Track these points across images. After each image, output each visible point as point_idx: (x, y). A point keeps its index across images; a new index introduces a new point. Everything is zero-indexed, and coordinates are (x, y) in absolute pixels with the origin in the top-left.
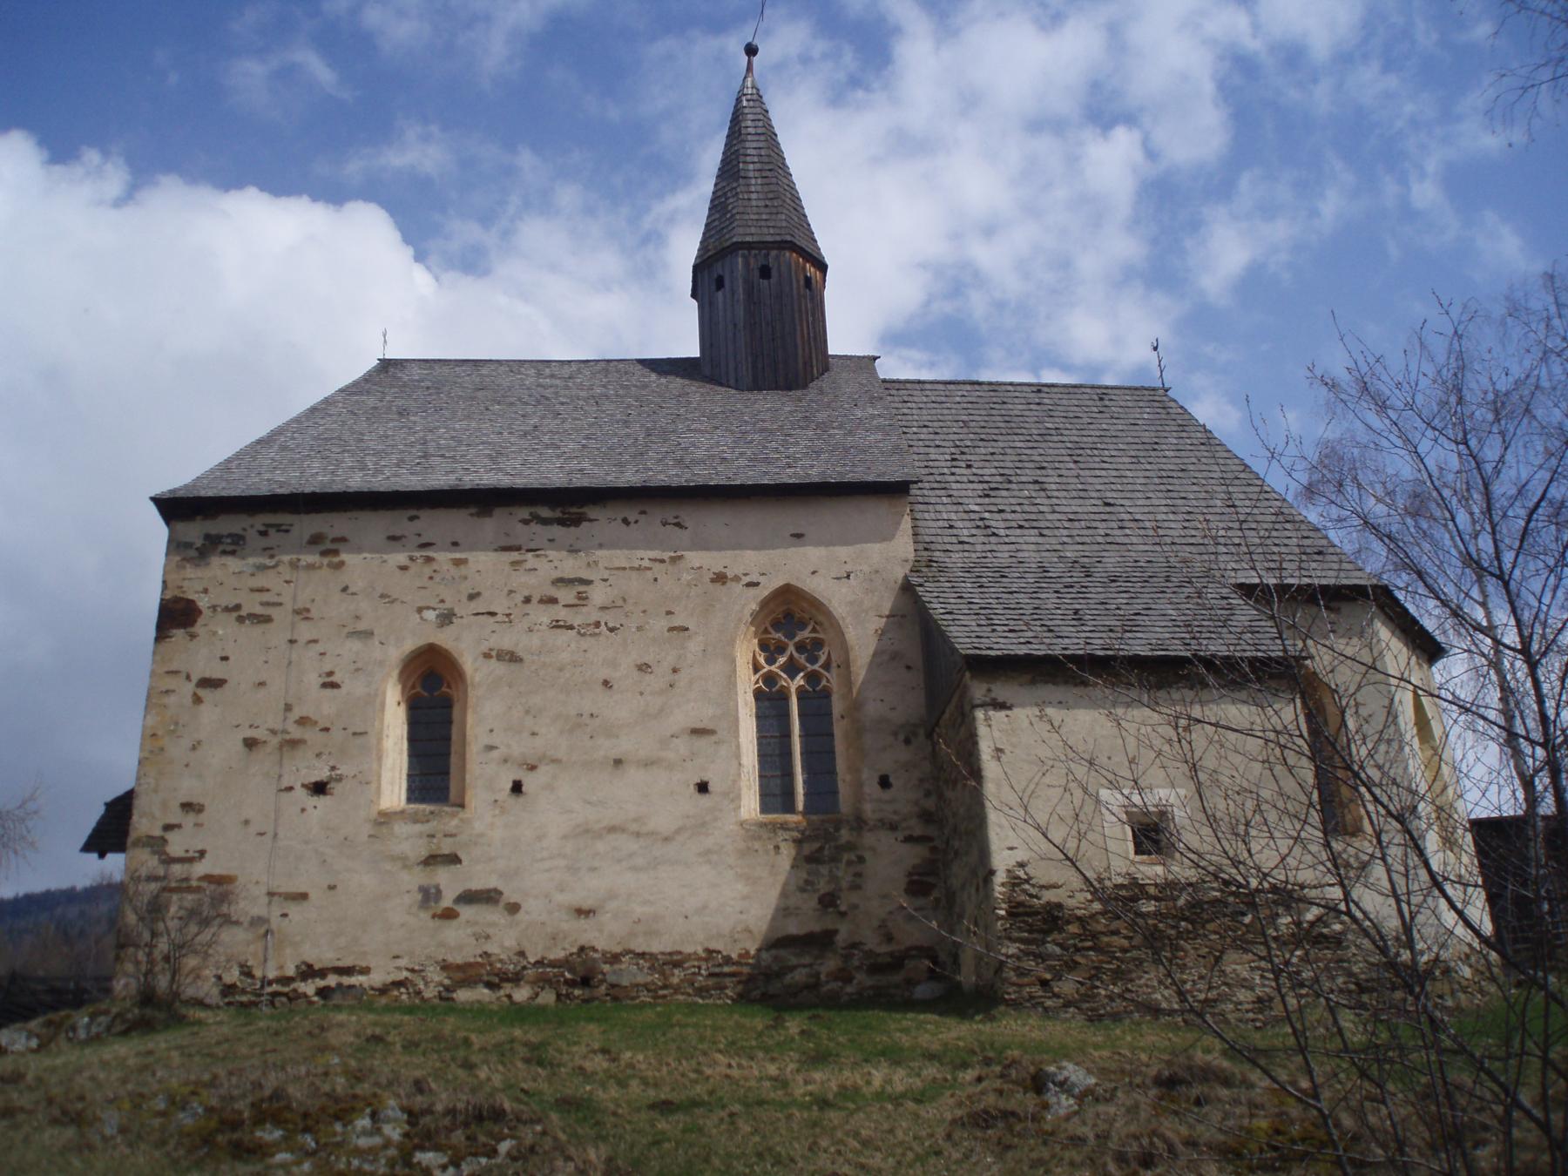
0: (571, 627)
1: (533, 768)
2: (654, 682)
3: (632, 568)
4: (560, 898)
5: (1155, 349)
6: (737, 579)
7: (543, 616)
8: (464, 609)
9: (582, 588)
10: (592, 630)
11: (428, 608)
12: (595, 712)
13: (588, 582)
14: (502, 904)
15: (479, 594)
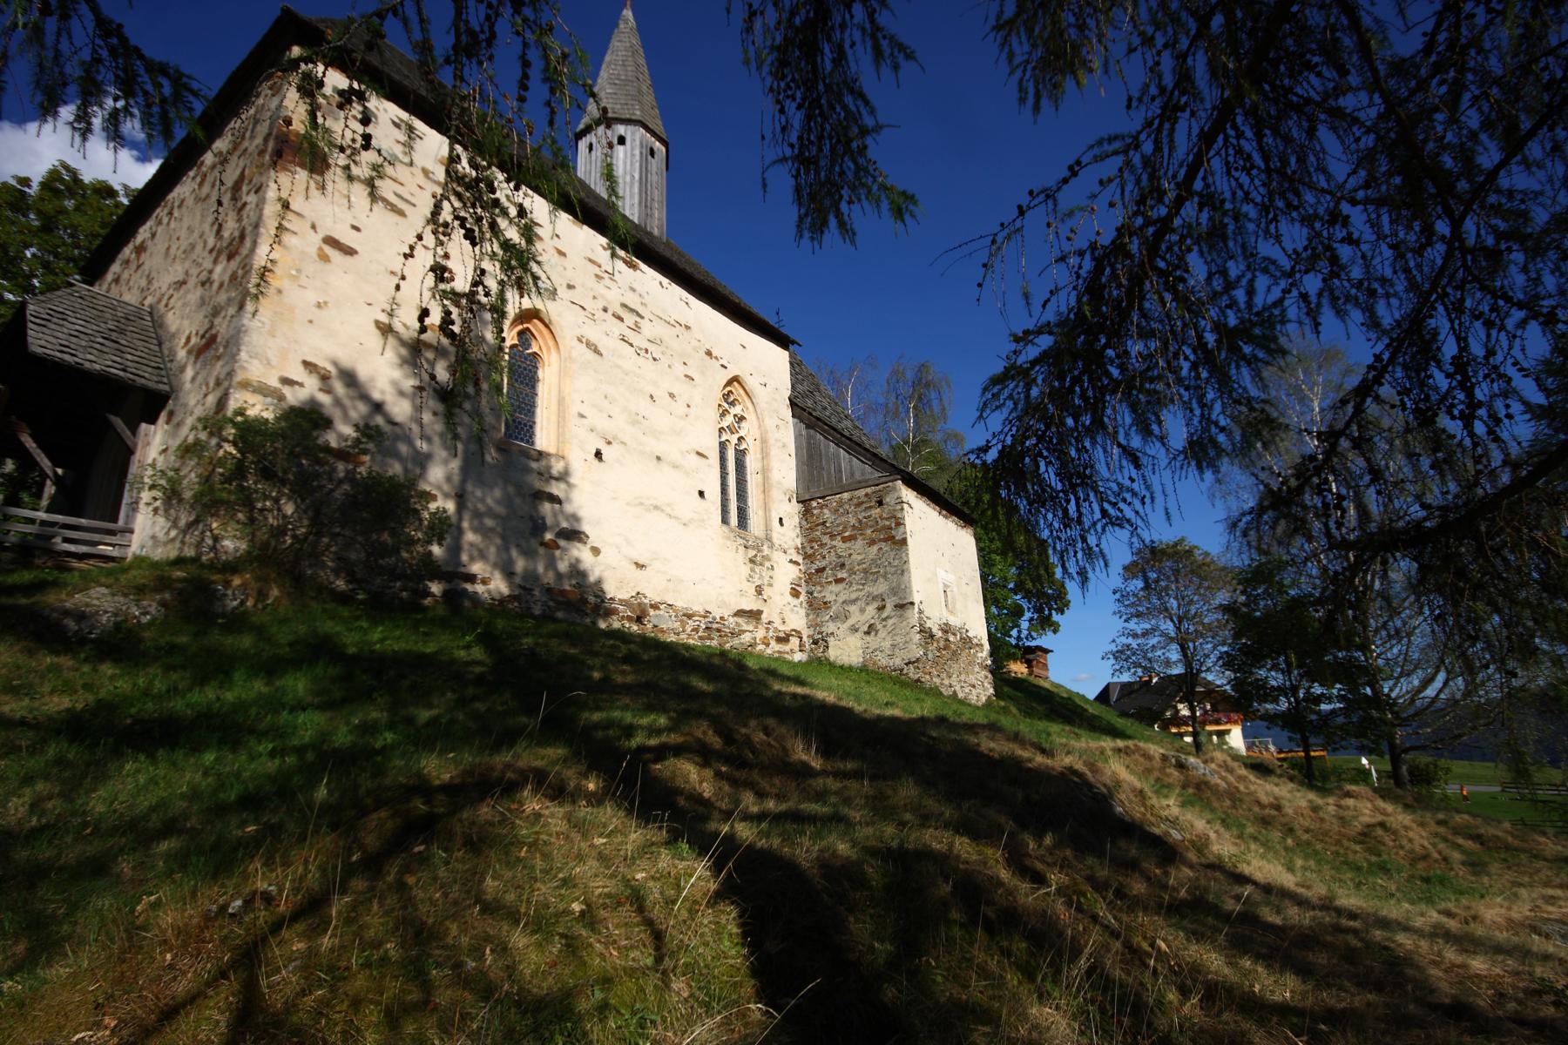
2: (679, 408)
7: (617, 328)
10: (642, 353)
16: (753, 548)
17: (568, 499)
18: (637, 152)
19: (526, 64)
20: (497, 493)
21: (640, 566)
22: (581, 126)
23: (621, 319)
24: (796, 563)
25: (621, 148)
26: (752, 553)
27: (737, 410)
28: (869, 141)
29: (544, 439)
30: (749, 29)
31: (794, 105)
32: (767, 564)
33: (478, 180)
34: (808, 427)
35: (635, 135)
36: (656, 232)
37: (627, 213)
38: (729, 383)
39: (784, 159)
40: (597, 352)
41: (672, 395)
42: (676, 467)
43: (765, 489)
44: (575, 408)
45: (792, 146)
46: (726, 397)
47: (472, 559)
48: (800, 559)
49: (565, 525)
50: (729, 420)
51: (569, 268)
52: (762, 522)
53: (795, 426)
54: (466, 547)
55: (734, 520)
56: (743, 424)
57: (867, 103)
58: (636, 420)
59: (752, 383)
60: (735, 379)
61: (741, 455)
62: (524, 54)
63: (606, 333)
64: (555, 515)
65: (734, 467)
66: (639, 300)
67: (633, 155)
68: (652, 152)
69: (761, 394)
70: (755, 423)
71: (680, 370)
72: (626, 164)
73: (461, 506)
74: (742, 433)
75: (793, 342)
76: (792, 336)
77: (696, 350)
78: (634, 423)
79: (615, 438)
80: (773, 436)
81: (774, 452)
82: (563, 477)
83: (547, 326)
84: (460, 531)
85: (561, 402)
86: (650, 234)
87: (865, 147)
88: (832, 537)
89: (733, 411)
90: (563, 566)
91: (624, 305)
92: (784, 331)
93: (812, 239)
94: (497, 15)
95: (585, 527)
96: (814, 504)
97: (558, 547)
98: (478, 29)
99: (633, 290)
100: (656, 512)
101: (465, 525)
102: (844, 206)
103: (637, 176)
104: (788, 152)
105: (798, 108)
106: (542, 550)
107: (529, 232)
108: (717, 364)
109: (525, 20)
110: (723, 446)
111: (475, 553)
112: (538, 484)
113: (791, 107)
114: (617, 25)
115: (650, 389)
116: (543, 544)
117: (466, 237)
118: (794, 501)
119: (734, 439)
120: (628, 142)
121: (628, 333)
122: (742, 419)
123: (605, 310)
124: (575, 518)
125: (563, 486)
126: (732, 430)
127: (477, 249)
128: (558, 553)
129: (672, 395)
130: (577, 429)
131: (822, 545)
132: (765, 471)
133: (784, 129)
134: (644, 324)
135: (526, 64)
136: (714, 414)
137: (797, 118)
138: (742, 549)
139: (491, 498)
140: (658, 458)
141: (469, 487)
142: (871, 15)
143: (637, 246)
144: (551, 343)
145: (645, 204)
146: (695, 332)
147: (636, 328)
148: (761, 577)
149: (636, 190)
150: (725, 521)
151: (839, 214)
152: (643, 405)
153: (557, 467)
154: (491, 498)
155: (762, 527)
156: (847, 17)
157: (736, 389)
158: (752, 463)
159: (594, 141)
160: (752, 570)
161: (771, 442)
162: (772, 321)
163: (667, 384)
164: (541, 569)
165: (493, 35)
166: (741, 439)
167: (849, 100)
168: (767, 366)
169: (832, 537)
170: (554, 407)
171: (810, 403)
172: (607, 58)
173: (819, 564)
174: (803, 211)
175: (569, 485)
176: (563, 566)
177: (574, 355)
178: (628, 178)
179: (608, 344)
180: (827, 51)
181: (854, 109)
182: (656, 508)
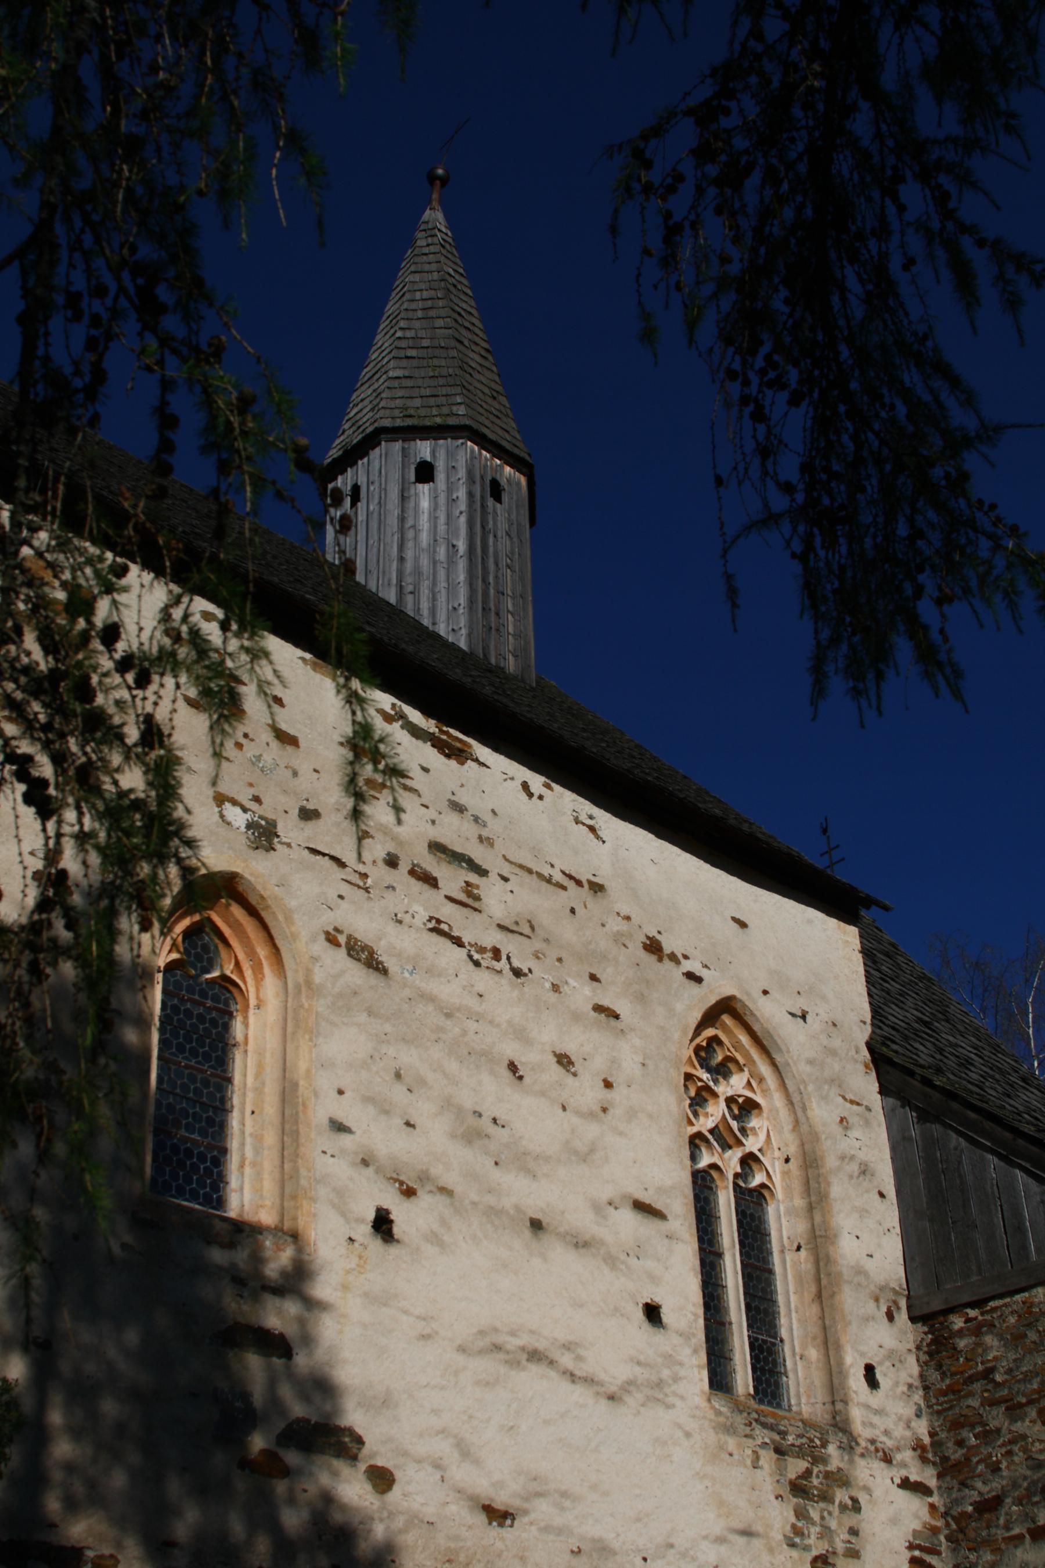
0: (458, 942)
1: (409, 1193)
2: (585, 1091)
3: (540, 875)
4: (462, 1474)
5: (825, 831)
6: (673, 957)
7: (422, 904)
8: (289, 829)
9: (473, 878)
10: (486, 960)
11: (234, 802)
12: (502, 1117)
13: (483, 873)
14: (362, 1467)
15: (870, 1110)
16: (800, 1452)
17: (308, 1340)
18: (461, 493)
19: (167, 421)
20: (132, 1337)
21: (498, 1515)
22: (334, 453)
23: (430, 881)
24: (918, 1488)
25: (424, 489)
26: (796, 1466)
27: (736, 1084)
28: (971, 461)
29: (249, 1191)
30: (669, 261)
31: (783, 396)
32: (841, 1496)
33: (55, 676)
34: (924, 1116)
35: (456, 459)
36: (511, 665)
37: (442, 630)
38: (710, 1017)
39: (770, 519)
40: (374, 964)
41: (564, 1061)
42: (581, 1244)
43: (824, 1285)
44: (323, 1108)
45: (788, 488)
46: (703, 1054)
47: (72, 1505)
48: (929, 1477)
49: (298, 1410)
50: (715, 1112)
51: (305, 768)
52: (818, 1378)
53: (889, 1116)
54: (57, 1475)
55: (743, 1379)
56: (754, 1122)
57: (955, 382)
58: (474, 1128)
59: (770, 1012)
60: (725, 1008)
61: (752, 1204)
62: (164, 404)
63: (395, 918)
64: (272, 1383)
65: (733, 1228)
66: (471, 830)
67: (452, 501)
68: (496, 490)
69: (797, 1042)
70: (784, 1114)
71: (581, 995)
72: (423, 531)
73: (43, 1373)
74: (752, 1144)
75: (869, 902)
76: (866, 887)
77: (620, 940)
78: (472, 1136)
79: (424, 1177)
80: (833, 1148)
81: (838, 1188)
82: (296, 1281)
83: (253, 912)
84: (39, 1436)
85: (289, 1094)
86: (498, 671)
87: (964, 477)
88: (1014, 1410)
89: (724, 1089)
90: (292, 1520)
91: (437, 848)
92: (842, 874)
93: (857, 693)
94: (109, 337)
95: (354, 1416)
96: (958, 1322)
97: (286, 1472)
98: (68, 370)
99: (459, 808)
100: (535, 1369)
101: (56, 1417)
102: (926, 610)
103: (462, 546)
104: (779, 502)
105: (795, 400)
106: (241, 1484)
107: (164, 776)
108: (676, 973)
109: (165, 341)
110: (703, 1183)
111: (79, 1488)
112: (234, 1306)
113: (777, 402)
114: (411, 242)
115: (510, 1050)
116: (245, 1464)
117: (28, 799)
118: (902, 1317)
119: (731, 1161)
120: (440, 476)
121: (448, 912)
122: (745, 1108)
123: (392, 862)
124: (322, 1387)
125: (292, 1307)
126: (723, 1137)
127: (51, 825)
128: (281, 1487)
129: (564, 1061)
130: (328, 1163)
131: (988, 1436)
132: (819, 1242)
133: (765, 452)
134: (491, 891)
135: (167, 421)
136: (671, 1101)
137: (794, 425)
138: (767, 1458)
139: (110, 1347)
140: (536, 1225)
141: (66, 1320)
142: (942, 198)
143: (467, 704)
144: (262, 952)
145: (483, 604)
146: (619, 900)
147: (469, 900)
148: (826, 1533)
149: (462, 577)
150: (719, 1379)
151: (915, 627)
152: (491, 1092)
153: (279, 1260)
154: (110, 1347)
155: (821, 1395)
156: (891, 209)
157: (734, 1038)
158: (783, 1222)
159: (362, 481)
160: (801, 1514)
161: (831, 1162)
162: (812, 855)
163: (550, 1034)
164: (237, 1528)
165: (99, 376)
166: (749, 1161)
167: (911, 377)
168: (804, 965)
169: (1014, 1410)
170: (271, 1109)
171: (924, 1053)
172: (391, 308)
173: (983, 1488)
174: (825, 634)
175: (312, 1304)
176: (292, 1520)
177: (318, 976)
178: (442, 553)
179: (401, 943)
180: (852, 282)
181: (927, 397)
182: (535, 1356)
